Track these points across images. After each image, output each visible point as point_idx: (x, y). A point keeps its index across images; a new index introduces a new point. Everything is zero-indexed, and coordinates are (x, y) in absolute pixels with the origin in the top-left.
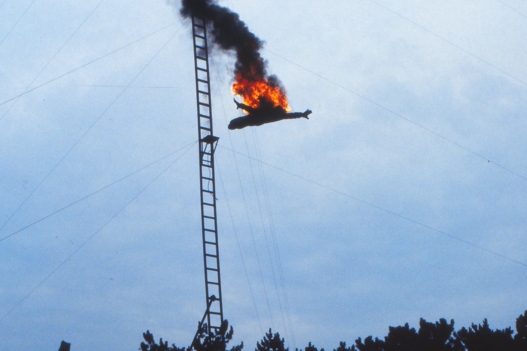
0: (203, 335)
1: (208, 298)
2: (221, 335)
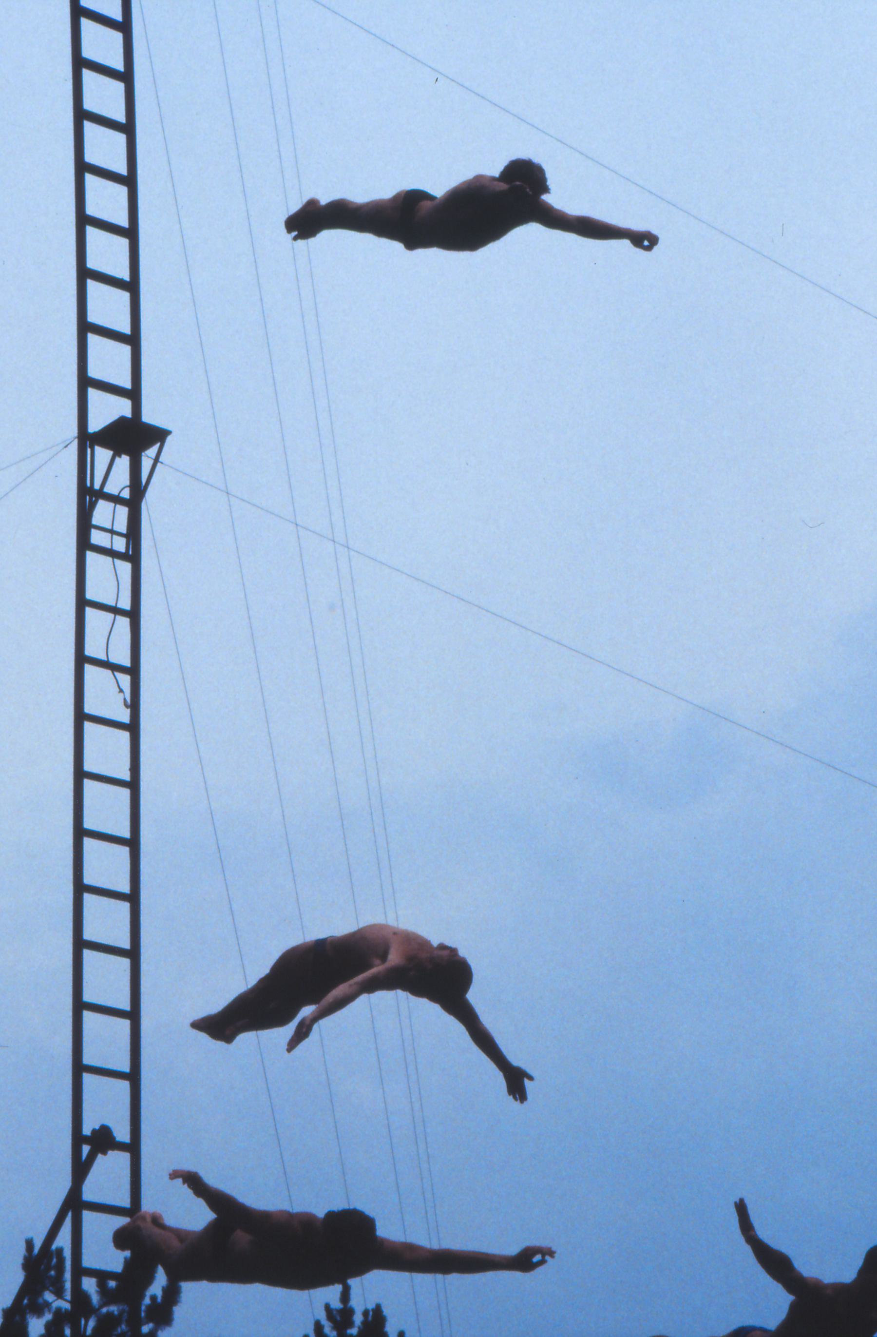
0: (40, 1300)
1: (78, 1139)
2: (126, 1308)
